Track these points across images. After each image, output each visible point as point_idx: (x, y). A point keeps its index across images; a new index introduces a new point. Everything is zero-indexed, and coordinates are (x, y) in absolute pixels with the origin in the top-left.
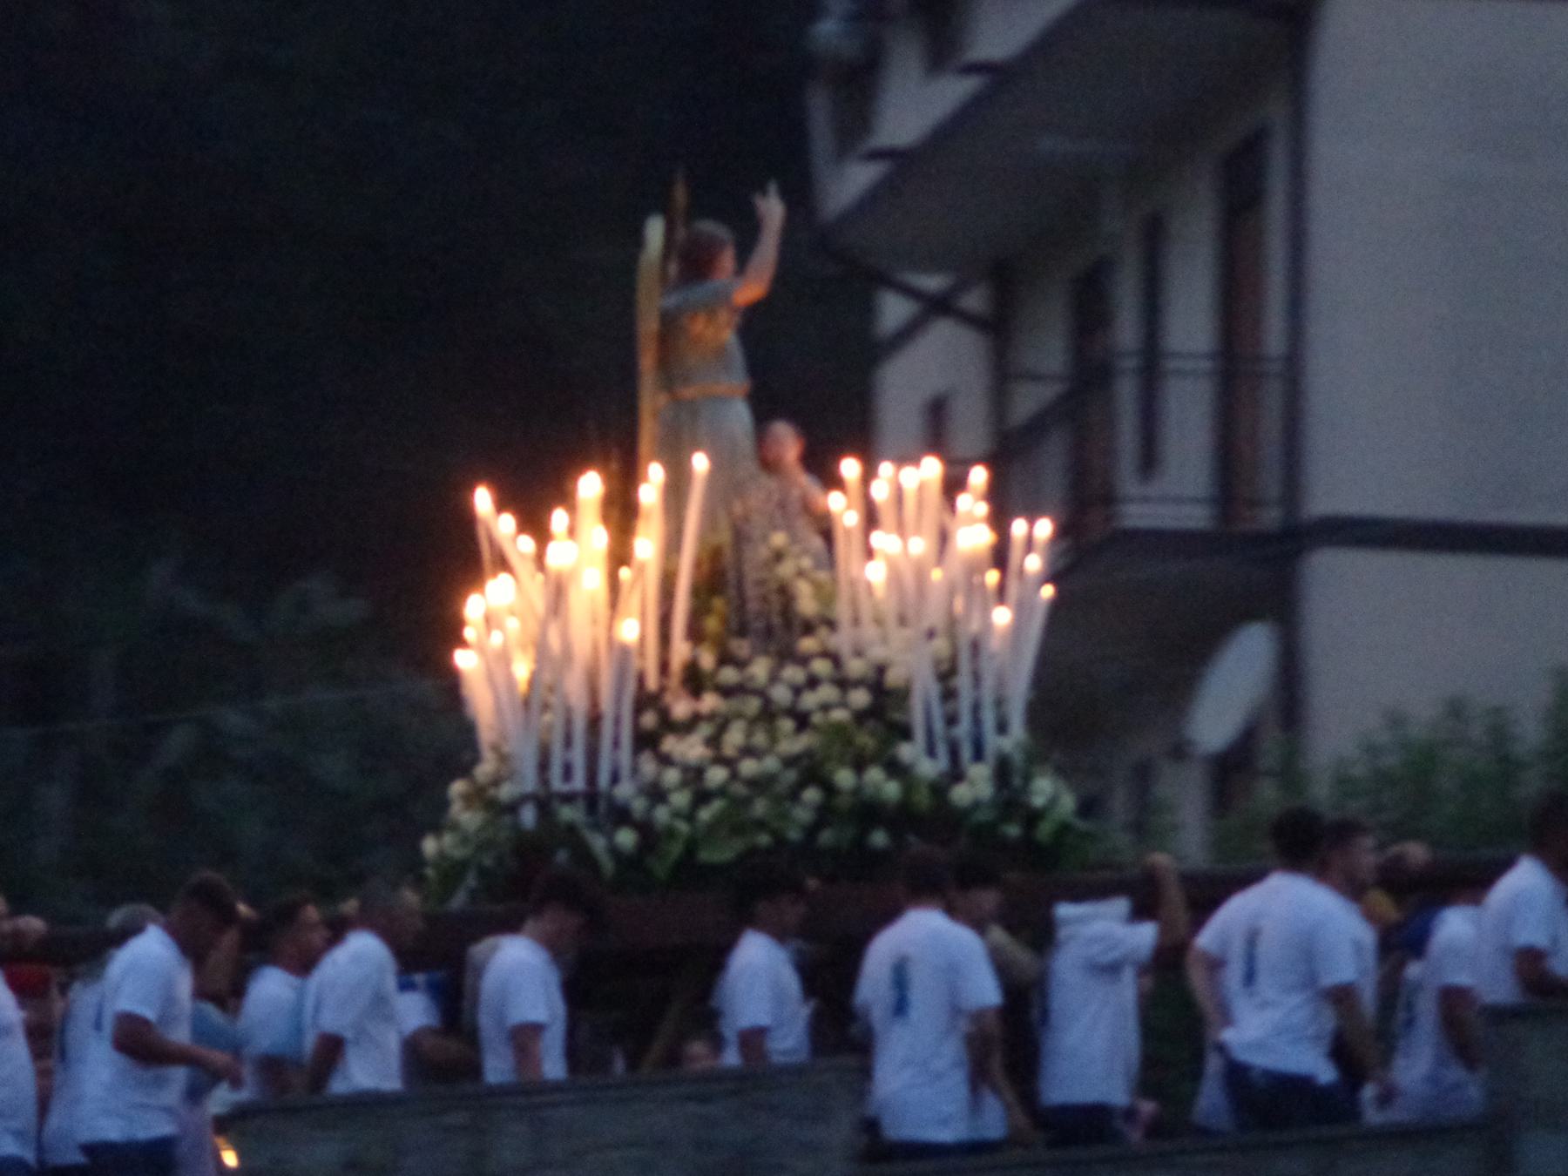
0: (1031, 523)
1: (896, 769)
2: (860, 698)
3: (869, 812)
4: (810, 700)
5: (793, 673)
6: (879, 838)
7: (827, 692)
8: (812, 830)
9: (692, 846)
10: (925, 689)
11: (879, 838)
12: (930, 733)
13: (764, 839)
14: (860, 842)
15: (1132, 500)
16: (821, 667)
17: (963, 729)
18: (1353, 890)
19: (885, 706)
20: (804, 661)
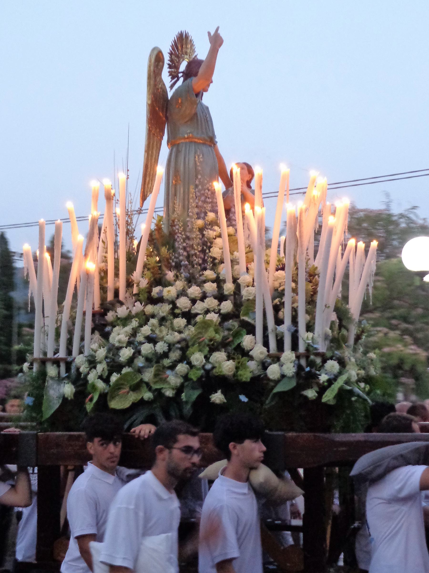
0: (357, 242)
1: (241, 353)
2: (227, 306)
3: (211, 381)
4: (199, 307)
5: (194, 291)
6: (218, 397)
7: (211, 302)
8: (179, 390)
9: (103, 397)
10: (264, 302)
11: (218, 397)
12: (265, 328)
13: (148, 395)
14: (204, 399)
15: (390, 378)
16: (210, 287)
17: (285, 328)
18: (335, 360)
19: (239, 314)
20: (200, 284)
